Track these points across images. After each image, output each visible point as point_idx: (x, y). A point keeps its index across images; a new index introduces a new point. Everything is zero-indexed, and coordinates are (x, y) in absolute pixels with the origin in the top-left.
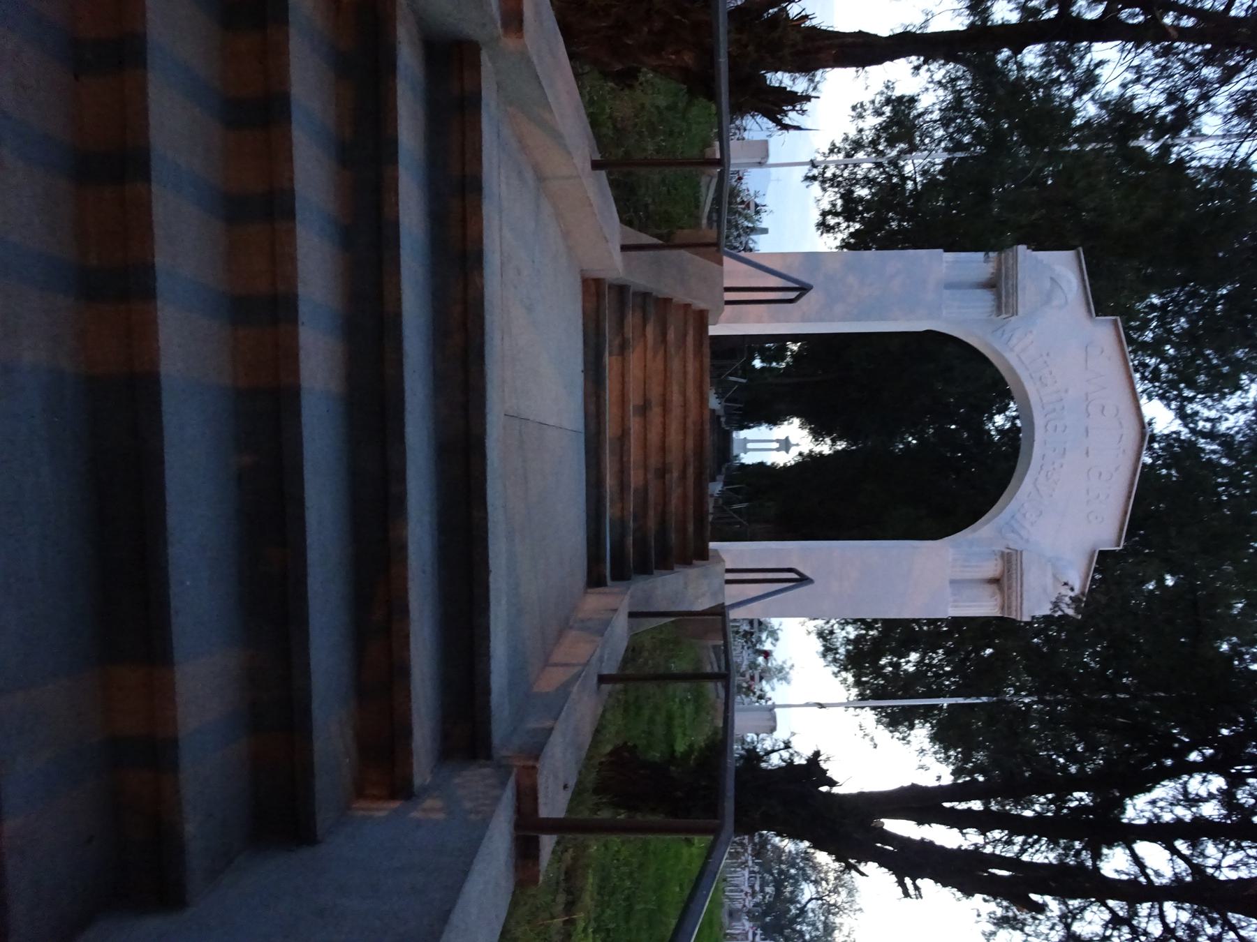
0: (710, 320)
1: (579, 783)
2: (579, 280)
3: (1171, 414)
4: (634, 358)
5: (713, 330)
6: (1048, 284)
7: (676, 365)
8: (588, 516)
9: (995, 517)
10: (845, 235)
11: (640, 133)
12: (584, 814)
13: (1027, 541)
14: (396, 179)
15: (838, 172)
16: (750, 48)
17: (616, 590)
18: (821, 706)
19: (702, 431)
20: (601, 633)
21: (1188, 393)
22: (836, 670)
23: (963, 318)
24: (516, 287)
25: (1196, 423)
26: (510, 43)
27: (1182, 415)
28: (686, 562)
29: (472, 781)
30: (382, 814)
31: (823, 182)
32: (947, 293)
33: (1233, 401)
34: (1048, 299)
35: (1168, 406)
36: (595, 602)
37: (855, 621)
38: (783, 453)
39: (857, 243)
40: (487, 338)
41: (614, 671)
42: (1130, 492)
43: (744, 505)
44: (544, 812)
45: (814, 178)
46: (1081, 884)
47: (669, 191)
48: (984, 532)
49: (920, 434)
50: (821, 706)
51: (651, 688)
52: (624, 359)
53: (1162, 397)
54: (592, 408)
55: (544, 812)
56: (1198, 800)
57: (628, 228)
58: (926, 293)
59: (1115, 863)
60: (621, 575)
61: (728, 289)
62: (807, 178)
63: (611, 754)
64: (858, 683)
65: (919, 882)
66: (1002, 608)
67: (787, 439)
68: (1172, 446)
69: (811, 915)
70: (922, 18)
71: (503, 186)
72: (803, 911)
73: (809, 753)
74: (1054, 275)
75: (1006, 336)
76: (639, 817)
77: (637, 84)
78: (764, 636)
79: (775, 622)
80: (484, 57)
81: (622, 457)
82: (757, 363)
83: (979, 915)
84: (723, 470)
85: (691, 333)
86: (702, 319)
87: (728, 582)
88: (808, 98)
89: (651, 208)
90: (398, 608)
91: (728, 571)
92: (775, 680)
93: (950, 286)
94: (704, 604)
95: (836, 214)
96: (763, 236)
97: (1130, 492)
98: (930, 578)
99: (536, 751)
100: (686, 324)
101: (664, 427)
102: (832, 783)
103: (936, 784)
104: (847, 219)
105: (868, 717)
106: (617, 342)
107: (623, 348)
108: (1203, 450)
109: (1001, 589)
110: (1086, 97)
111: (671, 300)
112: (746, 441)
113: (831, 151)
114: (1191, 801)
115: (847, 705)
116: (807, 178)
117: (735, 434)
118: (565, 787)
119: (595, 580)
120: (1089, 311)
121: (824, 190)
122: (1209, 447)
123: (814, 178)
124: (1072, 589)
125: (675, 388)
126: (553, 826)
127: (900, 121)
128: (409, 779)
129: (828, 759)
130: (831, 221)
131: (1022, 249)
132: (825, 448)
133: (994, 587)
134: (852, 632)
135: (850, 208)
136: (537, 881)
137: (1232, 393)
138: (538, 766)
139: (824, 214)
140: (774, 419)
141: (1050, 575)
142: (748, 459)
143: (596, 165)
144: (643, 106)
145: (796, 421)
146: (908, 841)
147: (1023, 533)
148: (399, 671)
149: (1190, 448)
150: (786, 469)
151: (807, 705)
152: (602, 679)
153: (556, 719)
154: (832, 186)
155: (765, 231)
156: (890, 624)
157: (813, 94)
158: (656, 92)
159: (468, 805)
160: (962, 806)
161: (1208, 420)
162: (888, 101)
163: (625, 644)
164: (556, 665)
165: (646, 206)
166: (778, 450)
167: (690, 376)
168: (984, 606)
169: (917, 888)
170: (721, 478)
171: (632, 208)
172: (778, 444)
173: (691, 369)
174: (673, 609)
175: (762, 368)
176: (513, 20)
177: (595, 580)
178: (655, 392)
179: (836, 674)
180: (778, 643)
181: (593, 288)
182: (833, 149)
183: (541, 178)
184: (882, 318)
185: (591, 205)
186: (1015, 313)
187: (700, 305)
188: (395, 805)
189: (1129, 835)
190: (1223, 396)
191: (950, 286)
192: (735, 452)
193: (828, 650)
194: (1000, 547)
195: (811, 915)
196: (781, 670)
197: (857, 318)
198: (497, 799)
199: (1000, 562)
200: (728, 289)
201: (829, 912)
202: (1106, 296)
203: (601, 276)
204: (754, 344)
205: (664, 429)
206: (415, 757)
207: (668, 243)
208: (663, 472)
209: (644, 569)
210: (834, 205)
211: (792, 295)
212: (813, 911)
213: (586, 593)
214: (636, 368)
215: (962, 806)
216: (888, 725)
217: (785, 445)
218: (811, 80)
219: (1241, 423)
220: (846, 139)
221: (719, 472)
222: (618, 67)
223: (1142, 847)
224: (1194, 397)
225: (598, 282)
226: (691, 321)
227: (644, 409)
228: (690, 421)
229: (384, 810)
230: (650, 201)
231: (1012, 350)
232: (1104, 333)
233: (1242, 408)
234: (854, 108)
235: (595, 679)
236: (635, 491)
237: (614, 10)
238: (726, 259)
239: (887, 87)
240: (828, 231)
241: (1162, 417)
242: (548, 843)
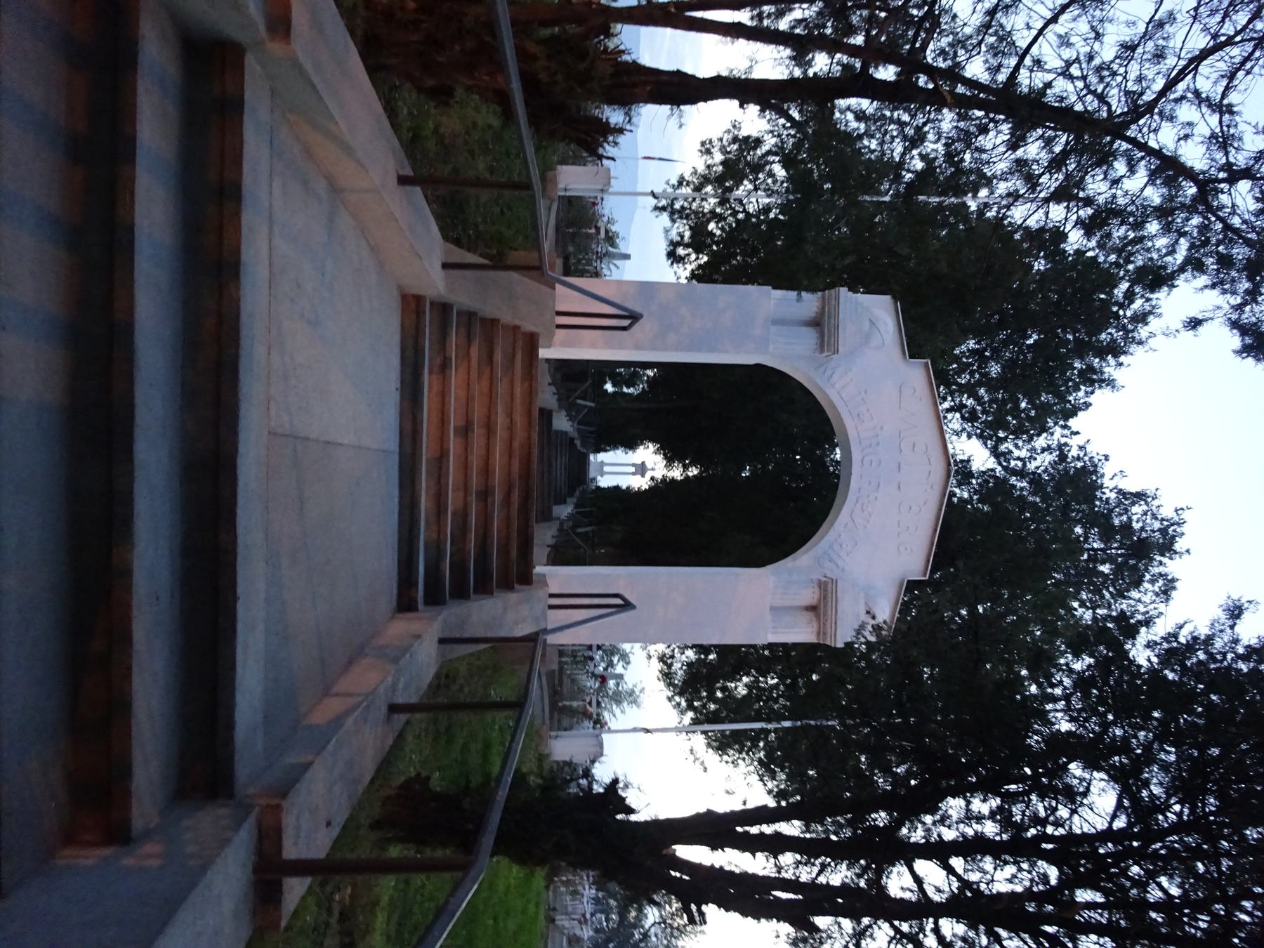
0: (541, 341)
1: (351, 818)
2: (395, 293)
3: (987, 453)
4: (455, 379)
5: (544, 353)
6: (867, 325)
7: (501, 388)
8: (400, 541)
9: (816, 544)
10: (694, 266)
11: (471, 152)
12: (364, 851)
13: (843, 570)
14: (132, 180)
15: (686, 205)
16: (559, 77)
17: (427, 615)
18: (648, 731)
19: (529, 454)
20: (395, 661)
21: (1001, 434)
22: (670, 694)
23: (787, 353)
24: (292, 300)
25: (1008, 461)
26: (275, 48)
27: (996, 453)
28: (507, 585)
29: (206, 820)
30: (90, 862)
31: (672, 213)
32: (774, 329)
33: (1040, 442)
34: (867, 339)
35: (985, 444)
36: (401, 627)
37: (693, 647)
38: (639, 477)
39: (701, 276)
40: (243, 352)
41: (414, 700)
42: (937, 525)
43: (589, 529)
44: (291, 851)
45: (663, 209)
46: (868, 903)
47: (502, 213)
48: (803, 561)
49: (757, 468)
50: (648, 731)
51: (464, 716)
52: (444, 378)
53: (980, 437)
54: (409, 427)
55: (291, 851)
56: (980, 818)
57: (452, 247)
58: (755, 328)
59: (898, 883)
60: (435, 598)
61: (559, 313)
62: (656, 208)
63: (402, 787)
64: (690, 707)
65: (704, 908)
66: (819, 633)
67: (643, 463)
68: (987, 482)
69: (654, 939)
70: (748, 64)
71: (277, 192)
72: (646, 936)
73: (607, 780)
74: (873, 317)
75: (828, 373)
76: (428, 853)
77: (452, 102)
78: (615, 659)
79: (626, 647)
80: (250, 61)
81: (439, 478)
82: (609, 387)
83: (778, 936)
84: (577, 493)
85: (519, 356)
86: (532, 342)
87: (551, 607)
88: (621, 131)
89: (481, 228)
90: (120, 638)
91: (552, 596)
92: (625, 704)
93: (776, 322)
94: (522, 630)
95: (687, 246)
96: (627, 262)
97: (937, 525)
98: (753, 604)
99: (284, 789)
100: (515, 342)
101: (488, 448)
102: (631, 811)
103: (743, 807)
104: (698, 251)
105: (699, 741)
106: (438, 361)
107: (444, 366)
108: (1014, 486)
109: (818, 617)
110: (915, 152)
111: (498, 320)
112: (602, 464)
113: (680, 183)
114: (970, 817)
115: (678, 730)
116: (656, 208)
117: (592, 457)
118: (328, 824)
119: (405, 604)
120: (904, 353)
121: (674, 221)
122: (1019, 484)
123: (663, 209)
124: (874, 618)
125: (500, 410)
126: (301, 868)
127: (739, 162)
128: (126, 822)
129: (626, 786)
130: (681, 251)
131: (843, 291)
132: (677, 473)
133: (809, 615)
134: (690, 654)
135: (699, 240)
136: (278, 925)
137: (1039, 435)
138: (284, 804)
139: (674, 245)
140: (631, 444)
141: (862, 602)
142: (605, 482)
143: (403, 180)
144: (475, 124)
145: (652, 447)
146: (699, 867)
147: (839, 562)
148: (117, 708)
149: (1001, 483)
150: (640, 493)
151: (635, 730)
152: (394, 708)
153: (318, 754)
154: (681, 218)
155: (627, 257)
156: (723, 650)
157: (628, 127)
158: (470, 115)
159: (191, 849)
160: (754, 830)
161: (1018, 459)
162: (735, 140)
163: (432, 671)
164: (337, 695)
165: (476, 226)
166: (633, 474)
167: (518, 400)
168: (801, 633)
169: (702, 914)
170: (572, 501)
171: (455, 222)
172: (632, 468)
173: (518, 391)
174: (490, 635)
175: (614, 393)
176: (280, 25)
177: (405, 604)
178: (478, 414)
179: (670, 699)
180: (630, 667)
181: (412, 305)
182: (681, 182)
183: (335, 189)
184: (712, 350)
185: (396, 220)
186: (836, 351)
187: (528, 327)
188: (107, 852)
189: (909, 853)
190: (1031, 439)
191: (776, 322)
192: (592, 475)
193: (667, 676)
194: (816, 576)
195: (654, 939)
196: (631, 693)
197: (690, 349)
198: (226, 842)
199: (817, 589)
200: (559, 313)
201: (672, 935)
202: (917, 342)
203: (420, 292)
204: (606, 369)
205: (488, 450)
206: (134, 800)
207: (498, 263)
208: (485, 494)
209: (461, 593)
210: (682, 237)
211: (626, 323)
212: (656, 935)
213: (393, 618)
214: (456, 387)
215: (754, 830)
216: (718, 749)
217: (641, 469)
218: (627, 114)
219: (1046, 463)
220: (695, 172)
221: (571, 495)
222: (431, 83)
223: (921, 866)
224: (1007, 437)
225: (419, 299)
226: (520, 343)
227: (465, 431)
228: (516, 445)
229: (90, 858)
230: (480, 220)
231: (833, 386)
232: (916, 374)
233: (1048, 449)
234: (703, 144)
235: (384, 709)
236: (454, 514)
237: (424, 25)
238: (558, 286)
239: (734, 126)
240: (678, 262)
241: (980, 457)
242: (295, 889)
